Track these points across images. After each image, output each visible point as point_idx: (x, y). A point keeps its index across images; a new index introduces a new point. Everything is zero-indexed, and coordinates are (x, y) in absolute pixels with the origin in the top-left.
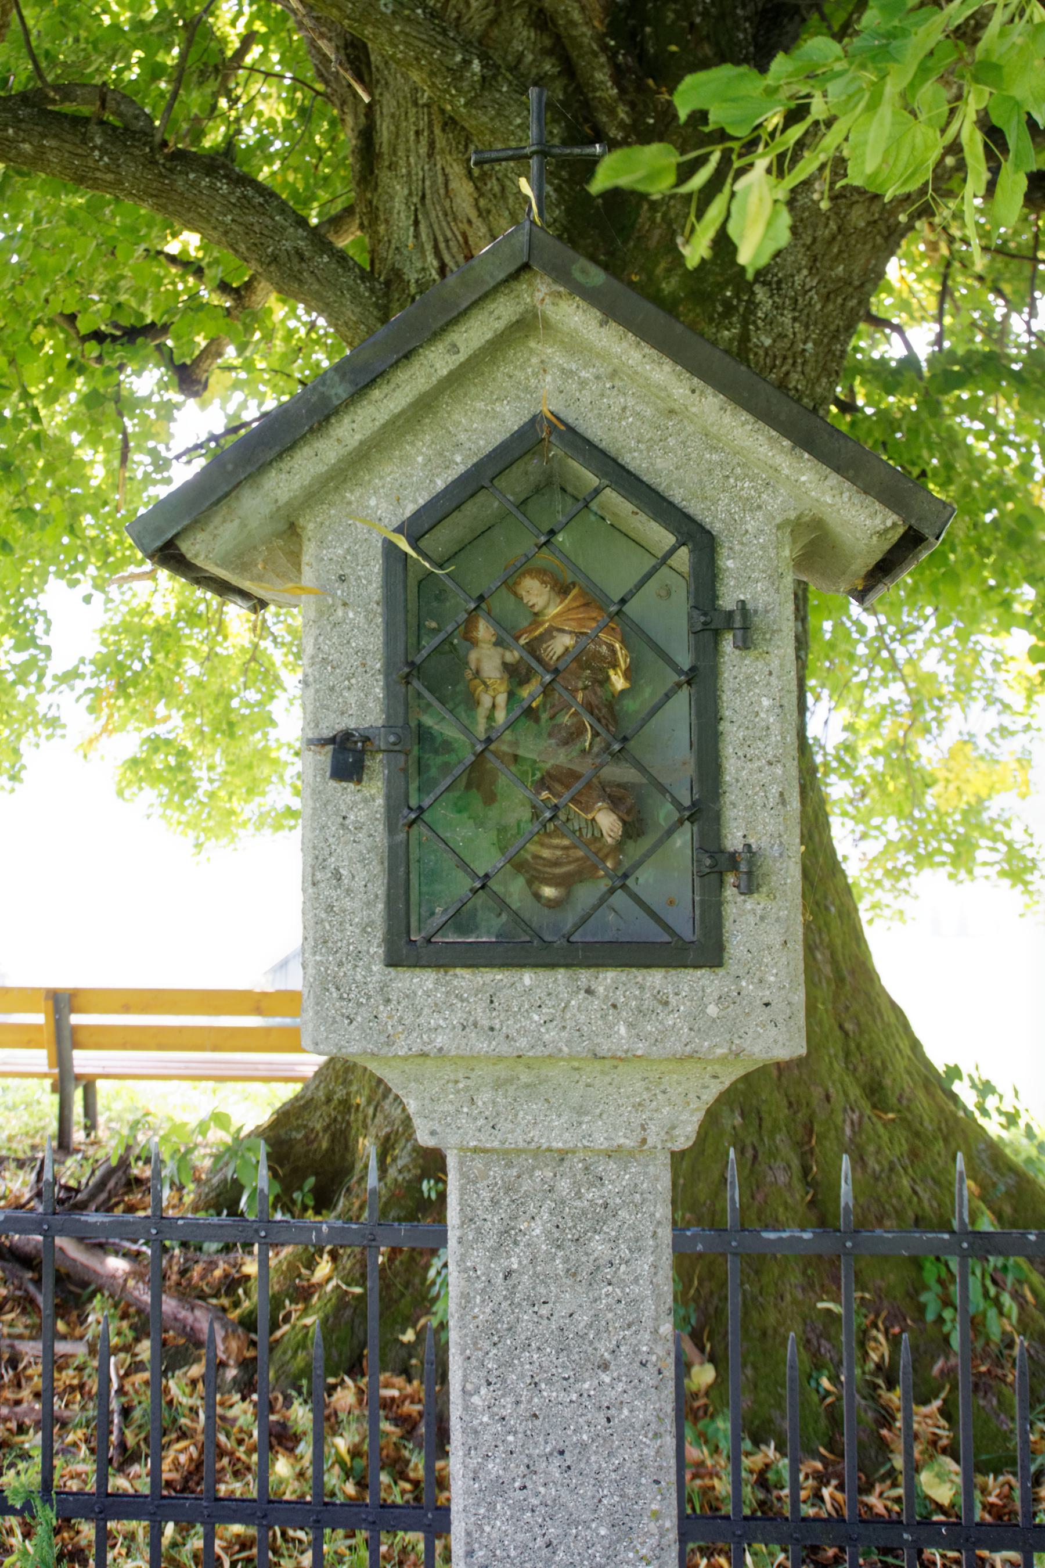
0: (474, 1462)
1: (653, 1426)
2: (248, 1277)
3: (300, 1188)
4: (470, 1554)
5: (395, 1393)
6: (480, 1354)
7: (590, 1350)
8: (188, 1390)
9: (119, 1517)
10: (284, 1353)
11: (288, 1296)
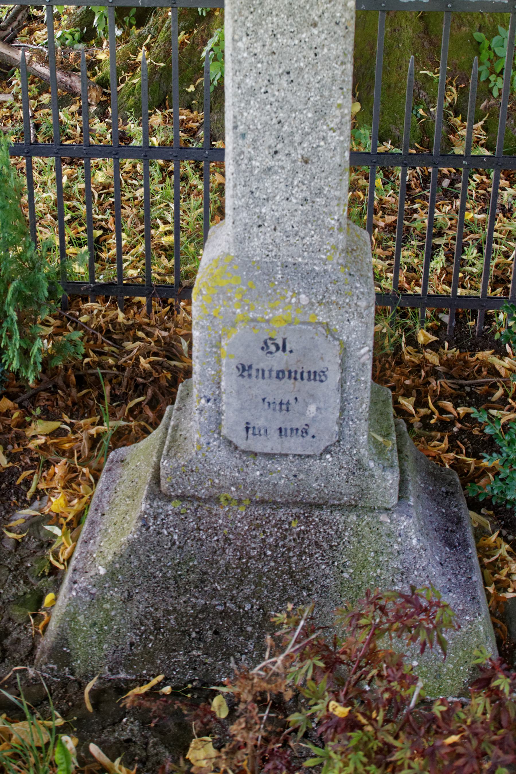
0: (238, 78)
1: (341, 58)
2: (100, 61)
3: (128, 15)
4: (235, 127)
5: (185, 117)
6: (243, 18)
7: (307, 15)
8: (70, 117)
9: (37, 155)
10: (122, 98)
11: (122, 69)
